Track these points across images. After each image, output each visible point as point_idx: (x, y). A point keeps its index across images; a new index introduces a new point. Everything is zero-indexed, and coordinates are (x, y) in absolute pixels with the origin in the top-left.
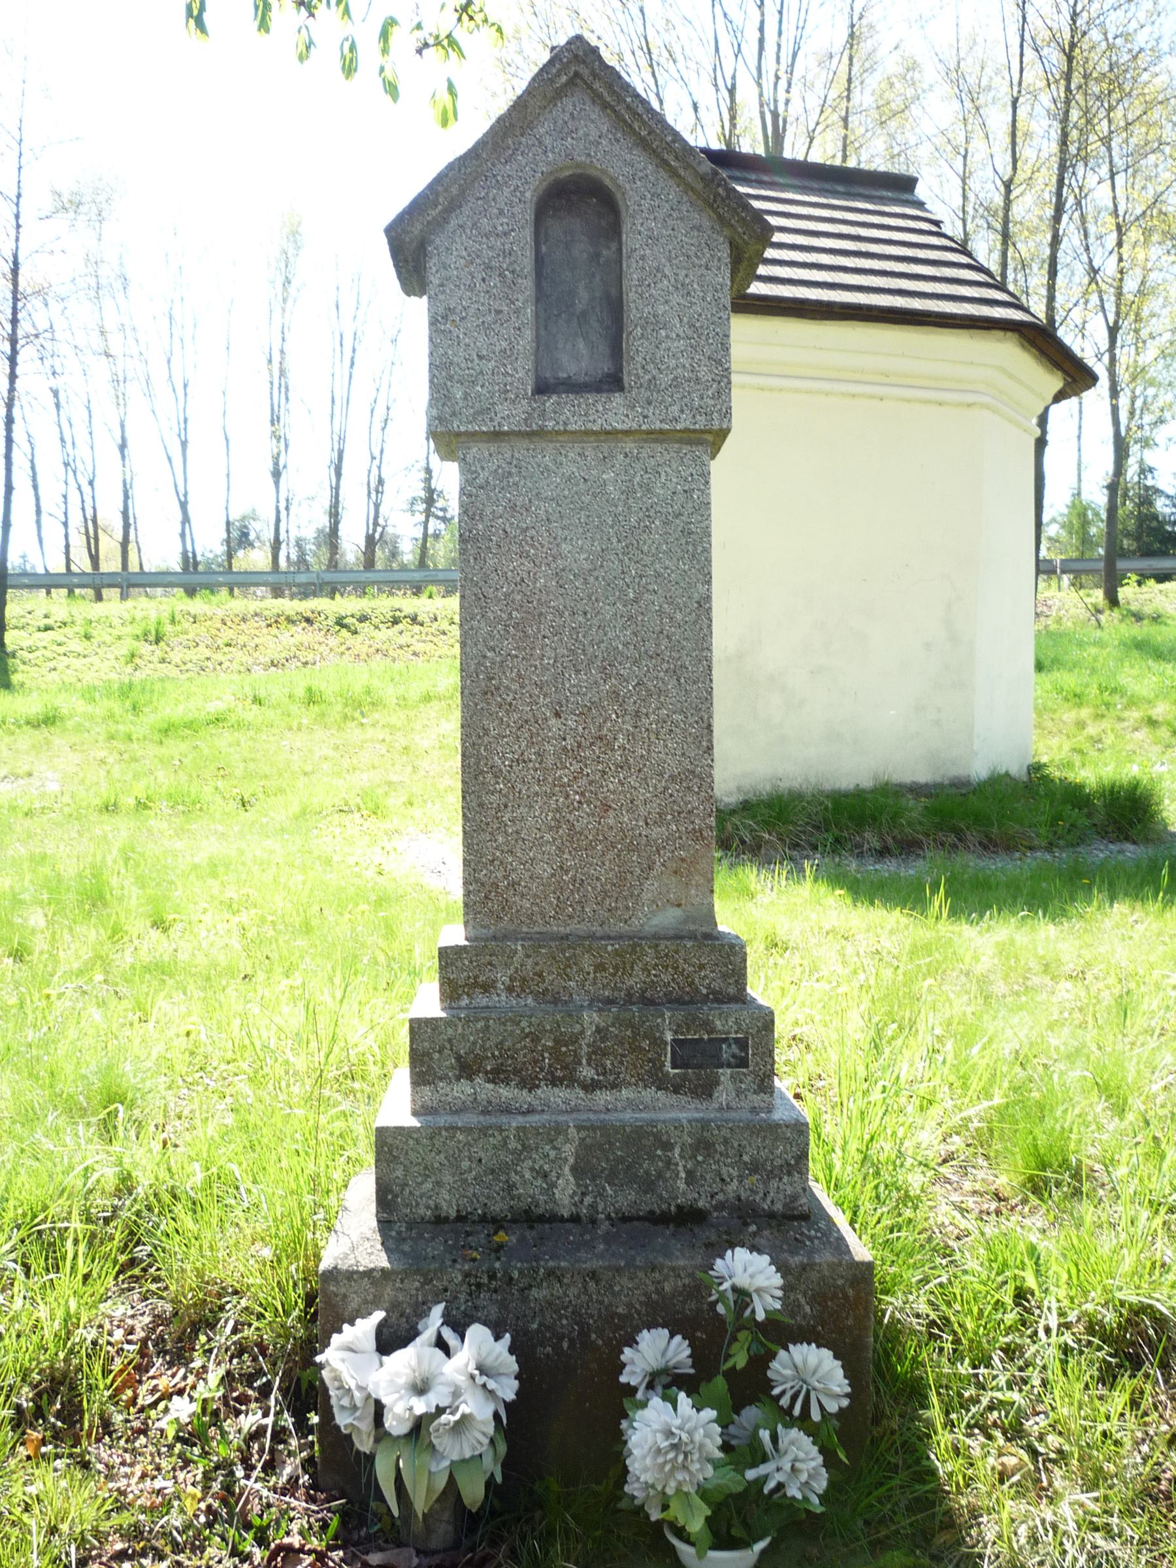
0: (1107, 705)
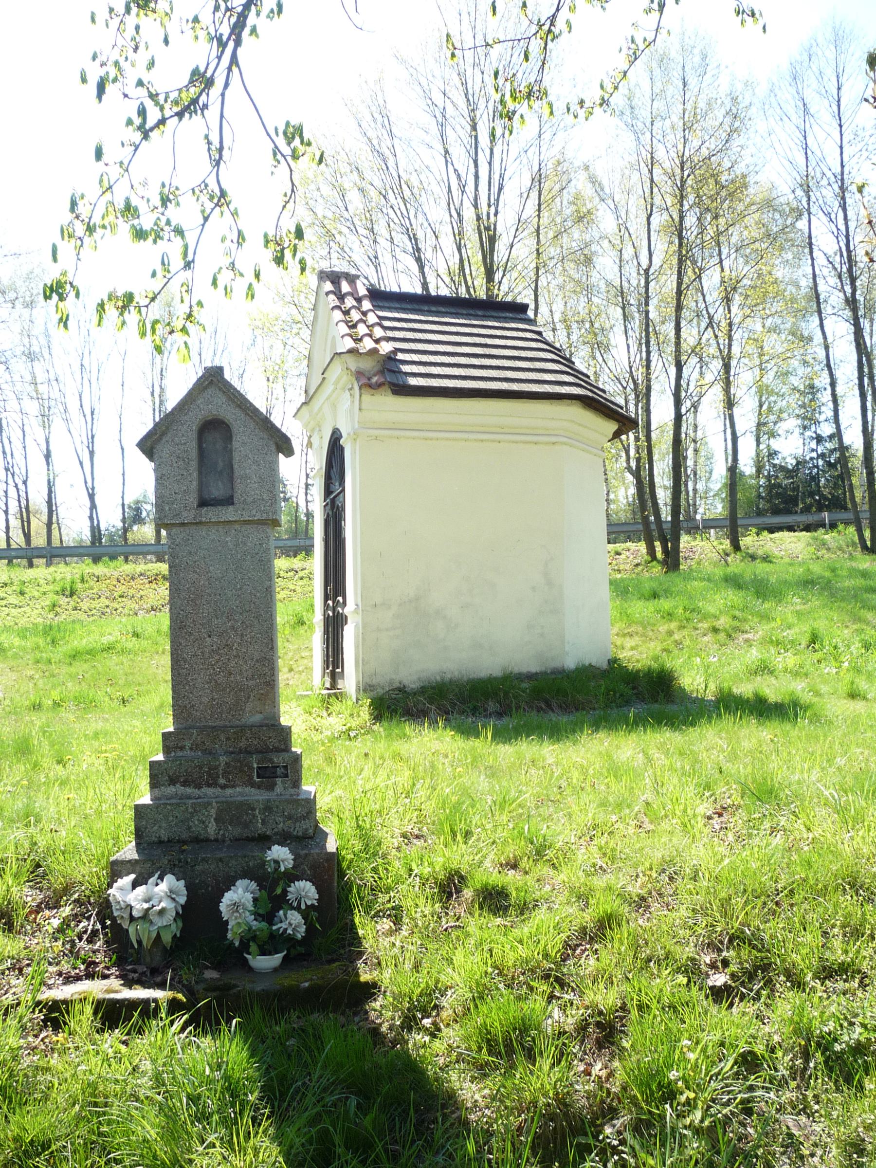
0: (688, 620)
